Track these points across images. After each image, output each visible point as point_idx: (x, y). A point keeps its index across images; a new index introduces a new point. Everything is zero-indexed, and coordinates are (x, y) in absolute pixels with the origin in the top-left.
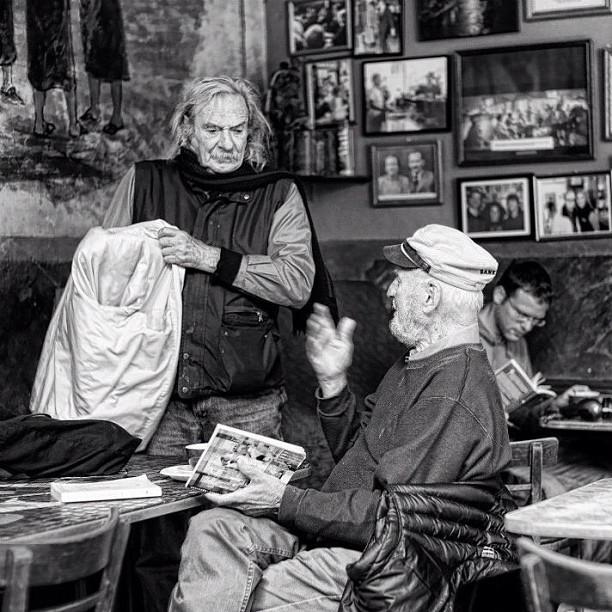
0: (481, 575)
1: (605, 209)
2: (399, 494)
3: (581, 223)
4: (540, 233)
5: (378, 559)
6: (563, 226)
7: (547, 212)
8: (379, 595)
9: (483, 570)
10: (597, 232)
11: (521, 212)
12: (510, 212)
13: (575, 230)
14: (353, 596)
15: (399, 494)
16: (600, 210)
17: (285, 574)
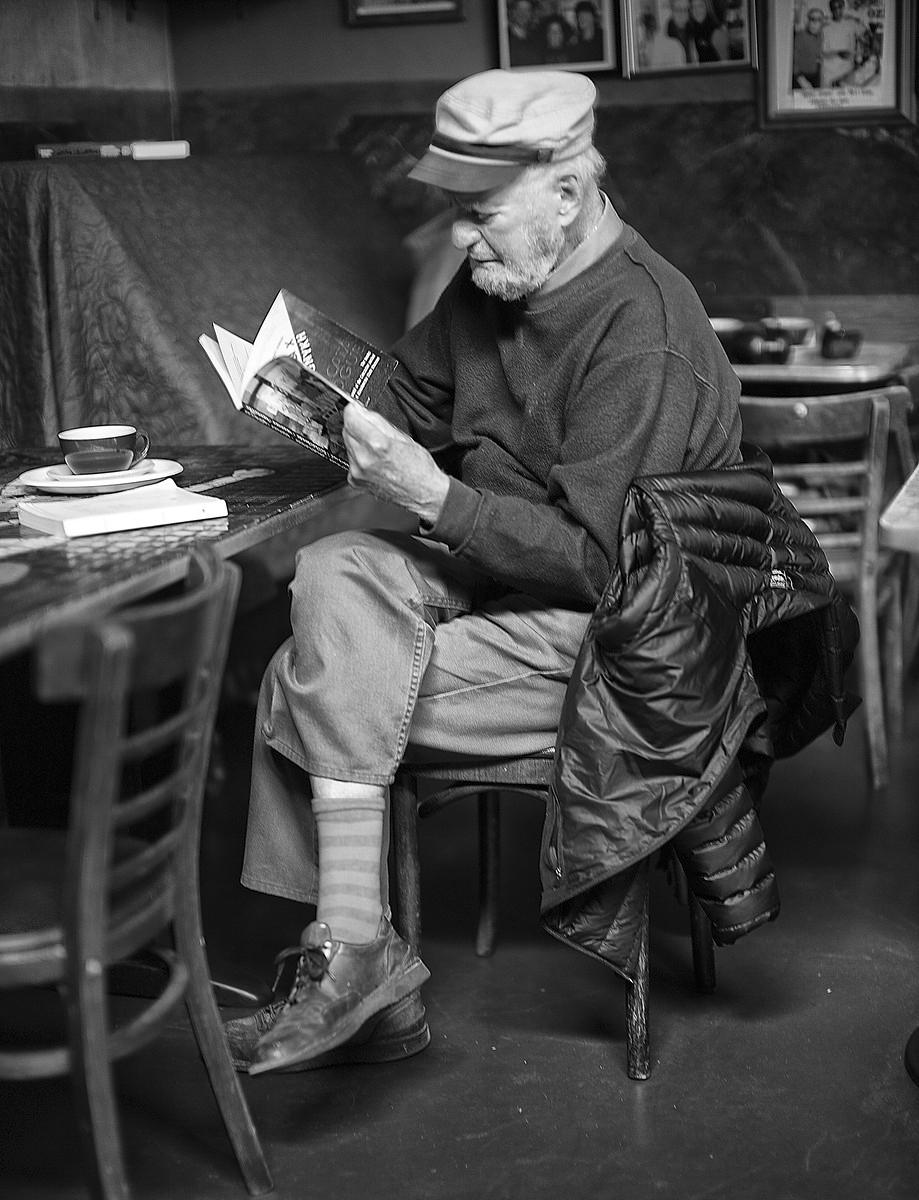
0: (774, 618)
1: (739, 24)
2: (661, 492)
3: (699, 49)
4: (631, 66)
5: (656, 604)
6: (669, 54)
7: (641, 30)
8: (660, 663)
9: (778, 607)
10: (725, 63)
11: (599, 32)
12: (581, 30)
13: (689, 60)
14: (596, 668)
15: (661, 492)
16: (731, 25)
17: (466, 637)
